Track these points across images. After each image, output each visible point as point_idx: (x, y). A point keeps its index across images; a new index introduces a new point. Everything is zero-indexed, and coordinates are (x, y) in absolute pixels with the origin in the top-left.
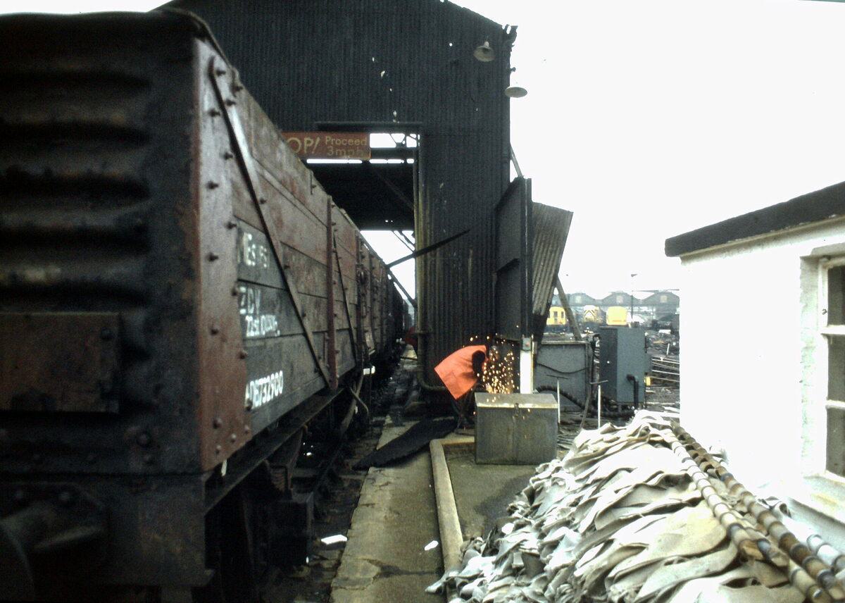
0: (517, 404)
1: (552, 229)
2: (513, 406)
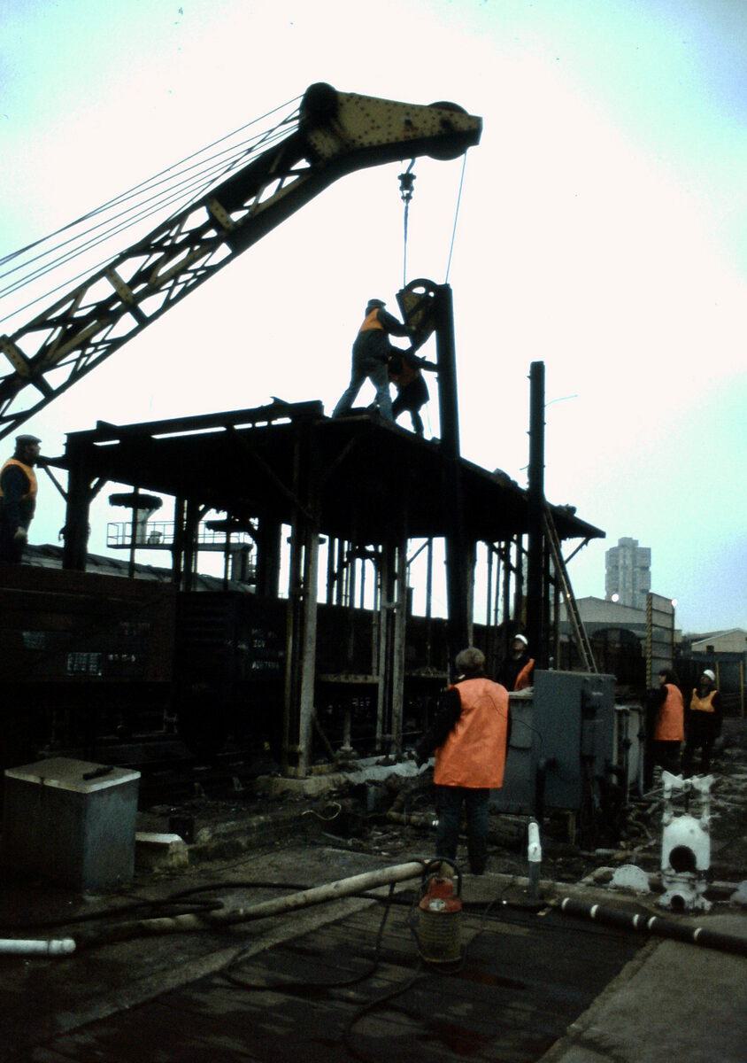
0: (42, 779)
1: (65, 444)
2: (37, 781)
